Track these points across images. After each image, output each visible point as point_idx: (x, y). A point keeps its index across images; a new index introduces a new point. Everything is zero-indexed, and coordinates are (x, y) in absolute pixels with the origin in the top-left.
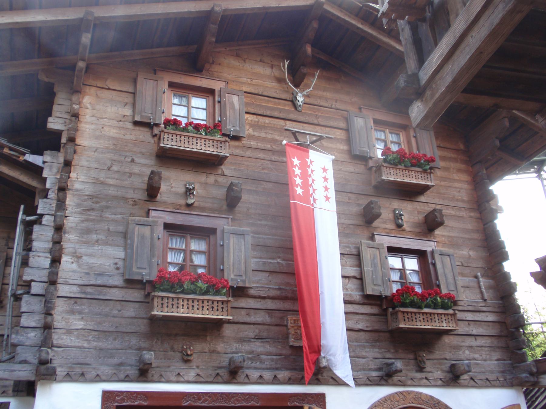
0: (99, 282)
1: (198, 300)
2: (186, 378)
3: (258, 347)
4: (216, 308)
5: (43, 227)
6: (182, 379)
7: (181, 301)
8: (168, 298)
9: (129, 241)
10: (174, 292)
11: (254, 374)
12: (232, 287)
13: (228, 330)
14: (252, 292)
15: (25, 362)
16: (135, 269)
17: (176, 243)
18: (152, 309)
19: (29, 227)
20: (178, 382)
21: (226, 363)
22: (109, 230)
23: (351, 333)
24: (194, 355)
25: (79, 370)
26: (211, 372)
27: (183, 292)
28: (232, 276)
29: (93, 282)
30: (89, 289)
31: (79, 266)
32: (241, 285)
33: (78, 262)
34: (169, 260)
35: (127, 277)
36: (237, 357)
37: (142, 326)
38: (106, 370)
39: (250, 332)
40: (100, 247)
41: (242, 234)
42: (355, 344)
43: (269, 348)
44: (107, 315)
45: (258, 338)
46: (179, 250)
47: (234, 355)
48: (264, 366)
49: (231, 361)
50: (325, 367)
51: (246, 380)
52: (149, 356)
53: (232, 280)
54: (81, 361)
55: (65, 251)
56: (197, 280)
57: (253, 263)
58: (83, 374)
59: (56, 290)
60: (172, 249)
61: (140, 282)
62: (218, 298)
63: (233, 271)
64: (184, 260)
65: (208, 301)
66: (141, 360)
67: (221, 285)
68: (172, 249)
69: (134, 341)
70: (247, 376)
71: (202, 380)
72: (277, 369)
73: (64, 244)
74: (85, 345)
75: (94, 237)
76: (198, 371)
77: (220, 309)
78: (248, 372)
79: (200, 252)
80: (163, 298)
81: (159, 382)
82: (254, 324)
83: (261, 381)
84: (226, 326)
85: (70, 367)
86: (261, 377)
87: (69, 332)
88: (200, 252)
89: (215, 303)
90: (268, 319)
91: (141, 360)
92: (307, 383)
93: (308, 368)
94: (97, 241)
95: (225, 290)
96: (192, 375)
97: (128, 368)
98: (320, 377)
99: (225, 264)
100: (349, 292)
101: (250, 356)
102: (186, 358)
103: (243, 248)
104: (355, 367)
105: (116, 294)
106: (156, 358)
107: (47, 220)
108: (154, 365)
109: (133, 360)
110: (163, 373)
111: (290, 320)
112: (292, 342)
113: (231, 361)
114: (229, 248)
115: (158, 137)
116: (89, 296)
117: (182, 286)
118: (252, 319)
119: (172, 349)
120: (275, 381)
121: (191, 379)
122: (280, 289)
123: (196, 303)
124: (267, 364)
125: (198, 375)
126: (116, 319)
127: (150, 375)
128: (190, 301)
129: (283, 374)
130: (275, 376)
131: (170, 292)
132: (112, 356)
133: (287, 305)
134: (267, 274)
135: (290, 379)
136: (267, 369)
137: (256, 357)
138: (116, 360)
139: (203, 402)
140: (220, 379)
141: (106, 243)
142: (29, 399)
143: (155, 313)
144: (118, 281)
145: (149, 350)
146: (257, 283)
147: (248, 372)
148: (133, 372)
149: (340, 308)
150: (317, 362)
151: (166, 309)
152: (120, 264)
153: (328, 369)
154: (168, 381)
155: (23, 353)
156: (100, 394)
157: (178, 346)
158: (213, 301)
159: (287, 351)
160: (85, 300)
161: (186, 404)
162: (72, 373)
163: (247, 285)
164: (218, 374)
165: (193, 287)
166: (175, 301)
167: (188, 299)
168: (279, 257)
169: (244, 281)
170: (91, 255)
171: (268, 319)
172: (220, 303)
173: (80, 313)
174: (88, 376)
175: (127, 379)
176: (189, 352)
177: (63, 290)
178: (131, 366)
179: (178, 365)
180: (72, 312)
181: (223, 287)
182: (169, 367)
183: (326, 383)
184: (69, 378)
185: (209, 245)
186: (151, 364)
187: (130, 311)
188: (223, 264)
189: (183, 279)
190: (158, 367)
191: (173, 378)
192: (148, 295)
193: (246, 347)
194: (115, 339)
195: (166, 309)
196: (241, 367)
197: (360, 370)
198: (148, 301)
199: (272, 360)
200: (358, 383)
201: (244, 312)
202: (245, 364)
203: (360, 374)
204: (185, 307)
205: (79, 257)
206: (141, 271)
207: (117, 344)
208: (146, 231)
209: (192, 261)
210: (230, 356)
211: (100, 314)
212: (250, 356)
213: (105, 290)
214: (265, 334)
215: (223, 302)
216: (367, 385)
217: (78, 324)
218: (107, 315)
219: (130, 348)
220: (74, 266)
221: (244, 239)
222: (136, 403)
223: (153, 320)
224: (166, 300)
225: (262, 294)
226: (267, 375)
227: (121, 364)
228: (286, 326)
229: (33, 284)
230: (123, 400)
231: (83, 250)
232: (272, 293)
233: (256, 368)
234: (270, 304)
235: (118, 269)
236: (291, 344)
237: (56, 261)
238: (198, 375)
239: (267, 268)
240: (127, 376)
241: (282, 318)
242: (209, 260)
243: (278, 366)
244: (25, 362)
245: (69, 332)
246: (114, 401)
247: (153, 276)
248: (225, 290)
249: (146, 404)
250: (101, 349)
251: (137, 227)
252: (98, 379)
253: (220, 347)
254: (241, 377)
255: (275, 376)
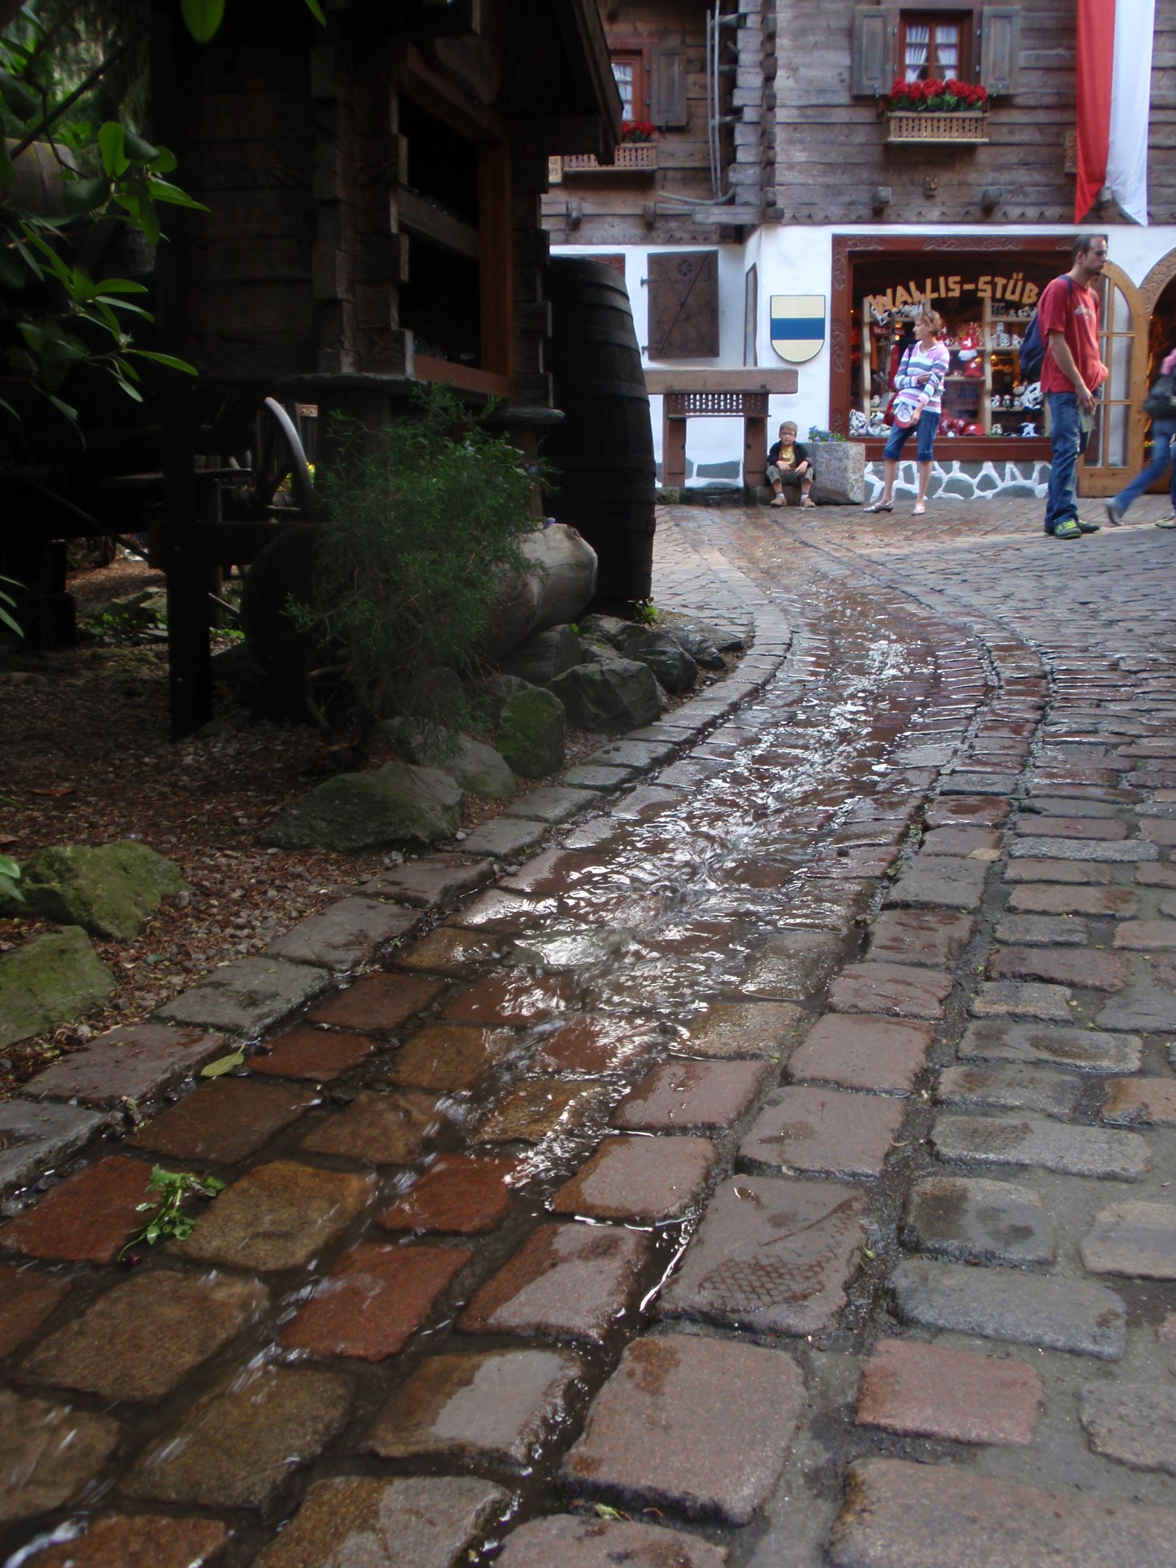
0: (821, 101)
1: (945, 119)
2: (929, 218)
3: (1022, 176)
4: (967, 128)
5: (748, 32)
6: (923, 220)
7: (923, 121)
8: (907, 119)
9: (856, 43)
10: (915, 111)
11: (1015, 212)
12: (990, 97)
13: (983, 157)
14: (1019, 101)
15: (746, 204)
16: (865, 82)
17: (916, 35)
18: (887, 132)
19: (729, 33)
20: (918, 223)
21: (978, 198)
22: (829, 27)
23: (1154, 152)
24: (939, 189)
25: (805, 212)
26: (959, 209)
27: (927, 110)
28: (991, 81)
29: (814, 101)
30: (810, 112)
31: (797, 81)
32: (1003, 92)
33: (794, 76)
34: (907, 62)
35: (856, 93)
36: (993, 190)
37: (876, 154)
38: (835, 211)
39: (1012, 156)
40: (820, 53)
41: (1008, 17)
42: (1160, 167)
43: (1037, 177)
44: (832, 143)
45: (1024, 164)
46: (920, 46)
47: (990, 188)
48: (1028, 200)
49: (985, 195)
50: (1107, 201)
51: (1004, 220)
52: (885, 192)
53: (991, 86)
54: (807, 200)
55: (780, 62)
56: (944, 92)
57: (1023, 58)
58: (810, 216)
59: (774, 116)
60: (911, 45)
61: (872, 97)
62: (970, 114)
63: (994, 72)
64: (927, 59)
65: (958, 119)
66: (875, 197)
67: (975, 97)
68: (911, 45)
69: (865, 175)
70: (1005, 214)
71: (947, 219)
72: (1045, 204)
73: (778, 54)
74: (810, 181)
75: (811, 39)
76: (943, 209)
77: (973, 129)
78: (1008, 209)
79: (948, 46)
80: (901, 119)
81: (896, 223)
82: (1018, 145)
83: (1022, 220)
84: (981, 150)
85: (796, 208)
86: (1023, 215)
87: (791, 166)
88: (948, 46)
89: (967, 122)
90: (1038, 138)
91: (875, 197)
92: (1154, 209)
93: (1081, 202)
94: (816, 44)
95: (980, 103)
96: (935, 214)
97: (860, 207)
98: (1103, 213)
99: (983, 62)
100: (1162, 92)
101: (1011, 188)
102: (929, 193)
103: (1008, 37)
104: (1152, 199)
105: (842, 116)
106: (894, 194)
107: (752, 21)
108: (891, 203)
109: (865, 197)
110: (901, 213)
111: (1069, 137)
112: (1068, 167)
113: (985, 195)
114: (988, 39)
115: (1079, 525)
116: (810, 120)
117: (925, 102)
118: (1017, 138)
119: (912, 183)
120: (1042, 220)
121: (934, 219)
122: (1058, 94)
123: (942, 123)
124: (1032, 198)
125: (943, 213)
126: (843, 148)
127: (885, 214)
128: (935, 122)
129: (1052, 211)
130: (1042, 214)
131: (910, 110)
132: (841, 194)
133: (1066, 117)
134: (1039, 74)
135: (1061, 216)
136: (1032, 204)
137: (1019, 189)
138: (846, 199)
139: (950, 246)
140: (970, 218)
141: (827, 47)
142: (737, 247)
143: (892, 139)
144: (843, 98)
145: (885, 184)
146: (1027, 86)
147: (1008, 209)
148: (866, 212)
149: (1142, 115)
150: (1097, 194)
151: (905, 134)
152: (846, 75)
153: (1114, 203)
154: (907, 222)
155: (744, 194)
156: (830, 238)
157: (918, 178)
158: (964, 120)
159: (1061, 180)
160: (806, 127)
161: (928, 249)
162: (798, 215)
163: (1012, 92)
164: (967, 213)
165: (938, 100)
166: (917, 122)
167: (932, 119)
168: (1060, 45)
169: (1008, 87)
170: (810, 66)
171: (1038, 138)
172: (973, 122)
173: (802, 142)
174: (816, 218)
175: (859, 221)
176: (933, 186)
177: (781, 115)
178: (864, 204)
179: (918, 202)
180: (791, 142)
181: (978, 99)
182: (908, 205)
183: (1110, 222)
184: (796, 221)
185: (961, 35)
186: (887, 202)
187: (860, 137)
188: (979, 63)
189: (926, 92)
190: (895, 205)
191: (914, 219)
192: (880, 115)
193: (1006, 177)
194: (844, 173)
195: (905, 134)
196: (997, 204)
197: (1163, 203)
198: (881, 124)
199: (1040, 193)
200: (1154, 220)
201: (1005, 130)
202: (1002, 199)
203: (1161, 210)
204: (929, 129)
205: (795, 70)
206: (872, 82)
207: (846, 179)
208: (877, 24)
209: (937, 59)
210: (984, 188)
211: (824, 142)
212: (1011, 188)
213: (828, 111)
214: (1032, 158)
215: (977, 120)
216: (1168, 223)
217: (800, 156)
218: (832, 143)
219: (862, 183)
220: (791, 83)
221: (1011, 23)
222: (871, 248)
223: (889, 148)
224: (905, 122)
225: (1032, 102)
226: (1032, 212)
227: (852, 203)
228: (1062, 145)
229: (746, 109)
230: (855, 245)
231: (799, 59)
232: (1047, 100)
233: (1017, 204)
234: (1041, 117)
235: (843, 81)
236: (1067, 170)
237: (769, 79)
238: (943, 213)
239: (1041, 65)
240: (859, 217)
241: (1058, 135)
242: (960, 58)
243: (1046, 200)
244: (746, 204)
245: (791, 166)
246: (846, 245)
247: (888, 90)
248: (980, 103)
249: (881, 248)
250: (828, 186)
251: (866, 21)
252: (827, 221)
253: (973, 177)
254: (998, 215)
255: (1042, 214)
